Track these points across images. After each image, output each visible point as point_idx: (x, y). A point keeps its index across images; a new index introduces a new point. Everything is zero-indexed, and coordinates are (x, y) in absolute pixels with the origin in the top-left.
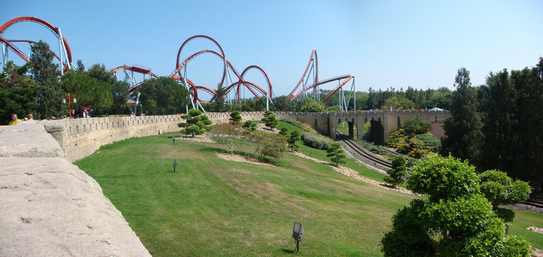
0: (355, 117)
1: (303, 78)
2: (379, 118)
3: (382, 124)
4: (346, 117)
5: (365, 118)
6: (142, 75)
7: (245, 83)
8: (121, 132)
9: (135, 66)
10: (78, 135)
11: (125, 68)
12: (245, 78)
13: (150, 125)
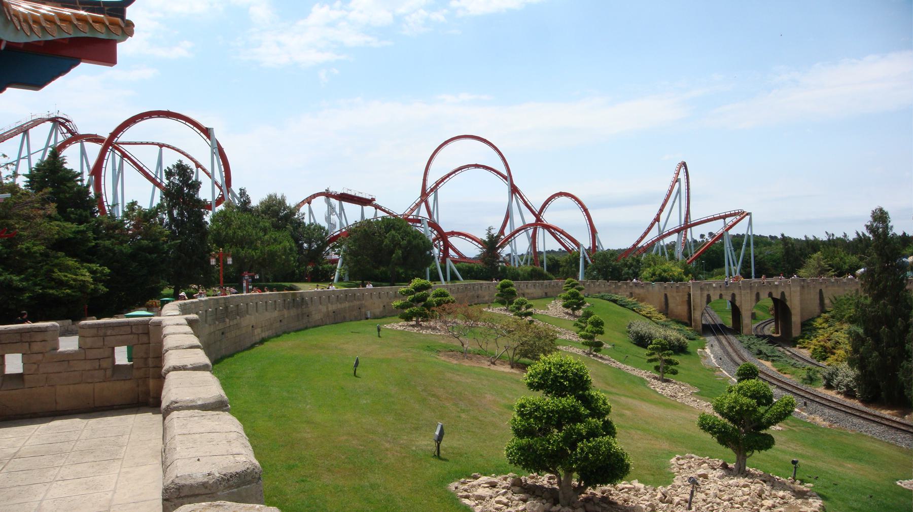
0: (736, 292)
1: (658, 215)
2: (783, 294)
3: (788, 303)
4: (721, 290)
5: (756, 293)
6: (358, 207)
7: (547, 227)
8: (298, 315)
9: (346, 192)
10: (227, 320)
11: (328, 195)
12: (548, 217)
13: (351, 304)
